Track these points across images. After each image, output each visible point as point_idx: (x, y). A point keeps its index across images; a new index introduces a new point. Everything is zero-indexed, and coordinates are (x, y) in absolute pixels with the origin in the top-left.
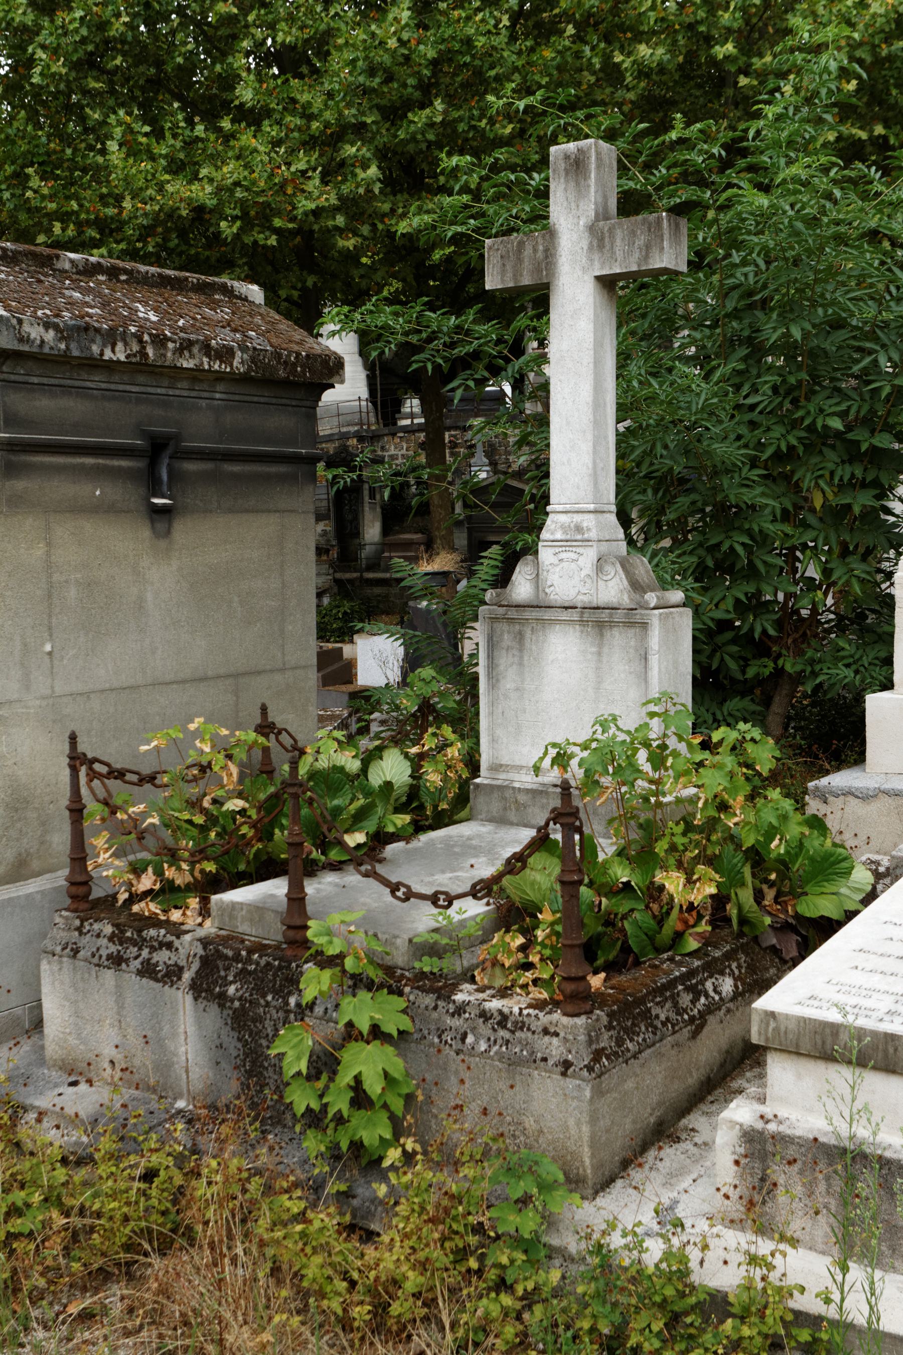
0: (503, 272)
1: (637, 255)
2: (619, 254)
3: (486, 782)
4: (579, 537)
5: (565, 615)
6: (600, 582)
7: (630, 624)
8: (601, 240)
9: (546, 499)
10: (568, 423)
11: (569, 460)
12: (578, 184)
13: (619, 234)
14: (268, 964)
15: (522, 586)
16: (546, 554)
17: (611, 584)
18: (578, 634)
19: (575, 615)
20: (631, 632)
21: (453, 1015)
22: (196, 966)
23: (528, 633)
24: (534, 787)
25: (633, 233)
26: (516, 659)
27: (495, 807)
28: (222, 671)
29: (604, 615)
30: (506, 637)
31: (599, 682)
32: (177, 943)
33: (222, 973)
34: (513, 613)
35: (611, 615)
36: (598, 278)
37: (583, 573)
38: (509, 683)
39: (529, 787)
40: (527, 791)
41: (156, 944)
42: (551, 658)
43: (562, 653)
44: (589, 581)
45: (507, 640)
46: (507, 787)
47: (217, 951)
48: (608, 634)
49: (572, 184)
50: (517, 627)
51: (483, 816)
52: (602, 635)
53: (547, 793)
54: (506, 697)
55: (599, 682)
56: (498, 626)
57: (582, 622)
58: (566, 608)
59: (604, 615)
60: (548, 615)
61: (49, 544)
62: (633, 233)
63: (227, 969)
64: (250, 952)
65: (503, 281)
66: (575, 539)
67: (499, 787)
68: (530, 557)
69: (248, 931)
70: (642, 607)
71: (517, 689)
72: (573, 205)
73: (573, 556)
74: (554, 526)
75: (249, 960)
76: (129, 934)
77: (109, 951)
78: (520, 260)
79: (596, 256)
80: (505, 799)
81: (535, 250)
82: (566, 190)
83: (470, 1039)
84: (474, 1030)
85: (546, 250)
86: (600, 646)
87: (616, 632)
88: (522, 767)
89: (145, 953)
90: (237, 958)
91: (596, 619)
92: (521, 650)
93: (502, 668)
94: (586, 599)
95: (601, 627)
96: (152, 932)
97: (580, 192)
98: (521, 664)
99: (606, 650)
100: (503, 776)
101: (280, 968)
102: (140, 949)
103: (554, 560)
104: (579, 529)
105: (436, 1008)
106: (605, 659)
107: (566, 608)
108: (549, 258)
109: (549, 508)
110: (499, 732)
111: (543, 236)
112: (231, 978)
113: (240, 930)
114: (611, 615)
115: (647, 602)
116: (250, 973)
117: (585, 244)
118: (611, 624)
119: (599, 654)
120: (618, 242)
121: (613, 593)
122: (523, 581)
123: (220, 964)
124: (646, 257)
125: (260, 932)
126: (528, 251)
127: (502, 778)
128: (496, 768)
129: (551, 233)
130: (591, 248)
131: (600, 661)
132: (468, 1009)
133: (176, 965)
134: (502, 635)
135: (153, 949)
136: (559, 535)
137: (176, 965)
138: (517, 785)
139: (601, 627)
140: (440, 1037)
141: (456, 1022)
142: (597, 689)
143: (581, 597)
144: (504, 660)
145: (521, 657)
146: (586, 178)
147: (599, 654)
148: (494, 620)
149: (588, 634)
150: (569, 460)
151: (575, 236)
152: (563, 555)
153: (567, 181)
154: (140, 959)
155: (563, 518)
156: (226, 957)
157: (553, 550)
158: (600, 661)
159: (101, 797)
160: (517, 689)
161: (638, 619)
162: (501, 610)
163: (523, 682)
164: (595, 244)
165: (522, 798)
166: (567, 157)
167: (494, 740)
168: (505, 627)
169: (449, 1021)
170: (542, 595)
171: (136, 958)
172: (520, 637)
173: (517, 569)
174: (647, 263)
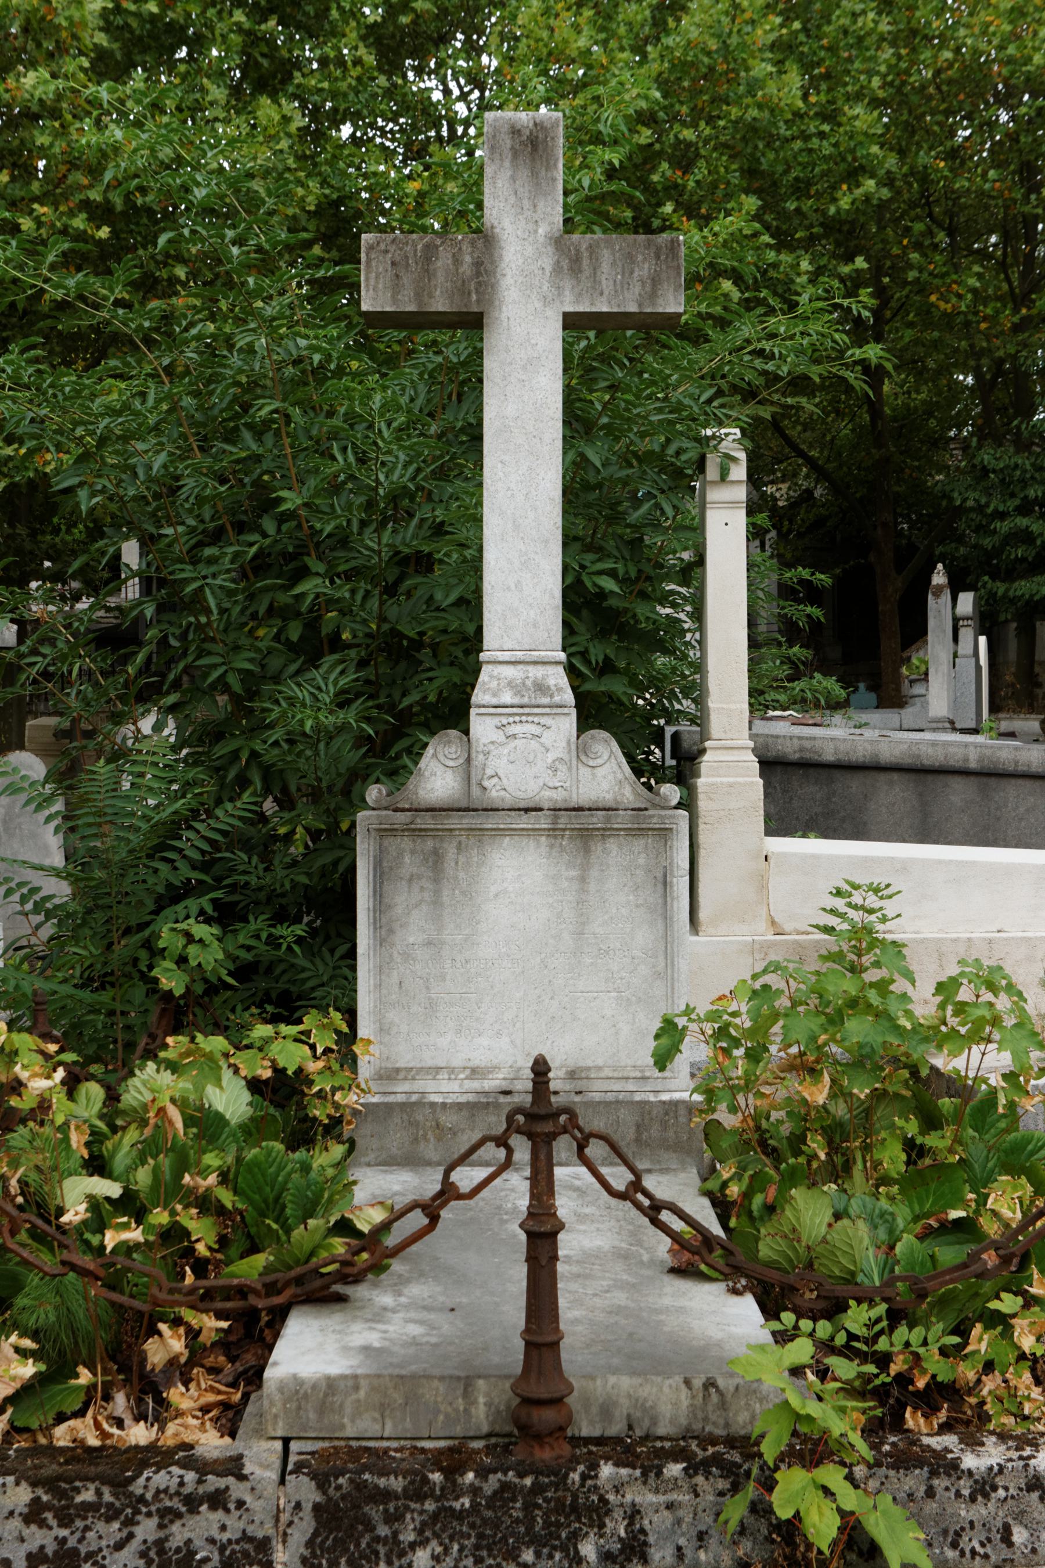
0: (396, 285)
1: (637, 289)
2: (606, 285)
4: (545, 700)
5: (524, 822)
6: (583, 771)
8: (575, 262)
9: (474, 641)
10: (517, 527)
11: (518, 585)
12: (534, 173)
13: (606, 256)
14: (505, 1486)
15: (437, 775)
16: (481, 727)
17: (600, 772)
18: (544, 850)
19: (543, 821)
20: (639, 844)
21: (973, 1499)
22: (303, 1529)
23: (450, 850)
25: (630, 258)
27: (396, 1139)
29: (597, 820)
30: (407, 860)
32: (238, 1490)
33: (383, 1531)
34: (425, 821)
35: (608, 820)
36: (566, 315)
37: (551, 757)
38: (413, 932)
40: (459, 1106)
41: (176, 1504)
42: (493, 889)
43: (515, 884)
44: (563, 768)
45: (409, 864)
46: (419, 1104)
47: (359, 1486)
48: (597, 848)
49: (524, 173)
50: (430, 843)
51: (371, 1157)
52: (587, 851)
54: (407, 957)
56: (393, 844)
57: (554, 832)
58: (527, 810)
59: (597, 820)
60: (490, 822)
62: (630, 258)
63: (394, 1518)
64: (452, 1472)
65: (394, 300)
66: (530, 706)
67: (403, 1106)
68: (453, 733)
69: (375, 1429)
71: (429, 943)
72: (526, 204)
74: (493, 686)
75: (452, 1489)
76: (88, 1496)
77: (33, 1546)
78: (428, 272)
79: (567, 284)
80: (415, 1124)
81: (457, 261)
82: (513, 179)
83: (1019, 1535)
84: (1020, 1516)
85: (478, 264)
86: (585, 868)
87: (612, 844)
88: (438, 1069)
89: (146, 1529)
90: (419, 1491)
92: (437, 881)
93: (399, 910)
95: (585, 836)
96: (161, 1479)
97: (538, 187)
98: (437, 903)
99: (594, 873)
100: (405, 1087)
101: (537, 1489)
102: (130, 1522)
103: (499, 736)
104: (541, 688)
105: (930, 1493)
106: (592, 887)
107: (527, 810)
108: (483, 273)
109: (483, 656)
110: (392, 1015)
111: (473, 243)
112: (408, 1536)
113: (350, 1432)
114: (608, 820)
115: (666, 799)
116: (460, 1515)
117: (547, 262)
118: (606, 833)
119: (583, 879)
120: (605, 267)
121: (605, 785)
122: (439, 770)
123: (374, 1512)
124: (653, 295)
125: (408, 1427)
126: (443, 260)
127: (401, 1091)
128: (390, 1075)
129: (484, 238)
130: (557, 269)
131: (583, 891)
132: (1000, 1481)
133: (245, 1537)
134: (400, 855)
135: (168, 1516)
136: (507, 698)
137: (245, 1537)
138: (438, 1099)
139: (585, 836)
140: (954, 1545)
141: (980, 1511)
142: (579, 934)
143: (547, 794)
144: (401, 898)
145: (437, 893)
146: (550, 167)
147: (583, 879)
148: (386, 832)
150: (518, 585)
151: (530, 250)
152: (517, 729)
153: (515, 166)
154: (135, 1545)
155: (509, 672)
156: (387, 1495)
157: (496, 721)
158: (583, 891)
159: (620, 1186)
160: (429, 943)
162: (402, 818)
164: (565, 264)
165: (448, 1120)
166: (515, 131)
168: (406, 843)
169: (965, 1512)
170: (476, 791)
171: (119, 1546)
172: (436, 859)
174: (654, 305)
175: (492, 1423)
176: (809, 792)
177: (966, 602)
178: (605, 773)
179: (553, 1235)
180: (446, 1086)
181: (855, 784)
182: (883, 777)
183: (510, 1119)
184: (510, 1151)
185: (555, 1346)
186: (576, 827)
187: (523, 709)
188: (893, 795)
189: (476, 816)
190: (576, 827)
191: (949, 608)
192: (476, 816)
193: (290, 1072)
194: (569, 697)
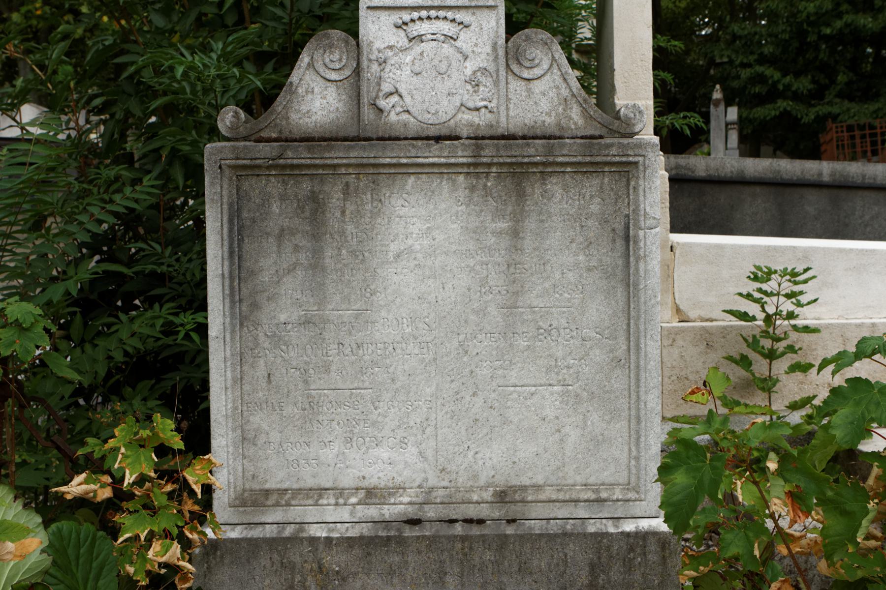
3: (234, 534)
5: (434, 155)
6: (516, 85)
7: (589, 168)
15: (315, 96)
17: (538, 87)
18: (462, 193)
24: (365, 530)
26: (303, 257)
28: (472, 135)
29: (534, 151)
31: (515, 292)
34: (298, 155)
35: (550, 151)
37: (470, 67)
38: (286, 306)
39: (354, 532)
40: (349, 542)
42: (394, 248)
46: (294, 540)
48: (535, 191)
50: (306, 186)
52: (521, 195)
53: (401, 541)
54: (277, 340)
55: (515, 292)
56: (254, 186)
57: (475, 169)
58: (438, 139)
61: (492, 502)
67: (272, 543)
70: (613, 133)
71: (307, 322)
73: (446, 28)
86: (518, 217)
87: (555, 186)
91: (504, 163)
93: (265, 277)
94: (481, 119)
98: (316, 266)
99: (531, 224)
103: (399, 39)
106: (528, 243)
107: (438, 139)
110: (258, 420)
114: (550, 151)
118: (547, 169)
119: (515, 233)
122: (318, 85)
127: (271, 522)
128: (254, 499)
134: (266, 200)
142: (510, 307)
143: (467, 117)
145: (317, 253)
147: (515, 233)
148: (245, 171)
149: (487, 192)
158: (516, 248)
160: (307, 322)
161: (614, 155)
162: (266, 150)
163: (321, 303)
165: (334, 560)
167: (246, 439)
168: (274, 186)
170: (368, 114)
172: (314, 209)
173: (305, 58)
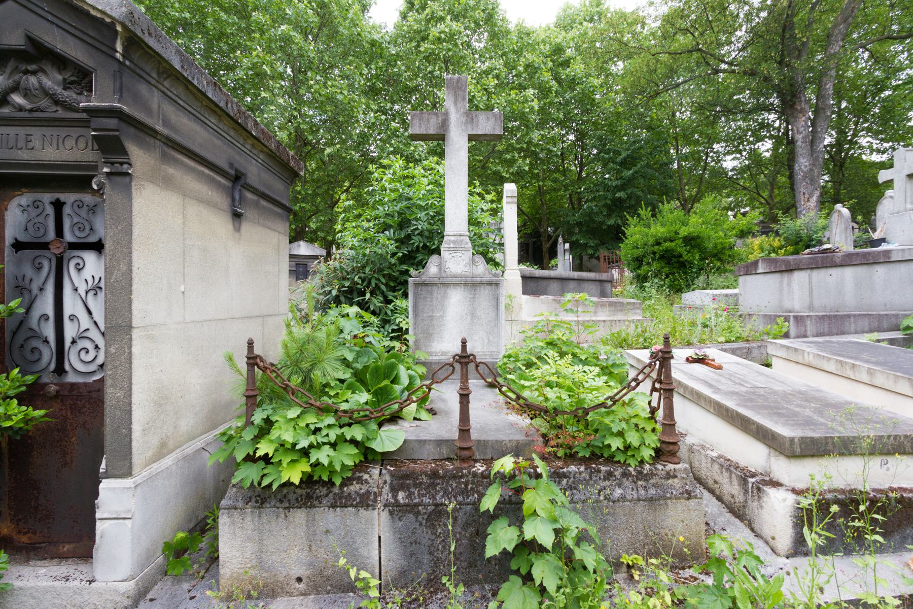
0: (420, 127)
15: (432, 267)
43: (455, 302)
155: (452, 238)
175: (445, 297)
176: (532, 284)
177: (567, 246)
178: (481, 268)
179: (468, 395)
180: (434, 358)
181: (544, 283)
182: (551, 281)
183: (454, 358)
184: (454, 368)
185: (468, 430)
186: (471, 284)
187: (455, 249)
188: (554, 286)
189: (444, 283)
190: (471, 284)
191: (563, 247)
192: (444, 283)
193: (491, 510)
194: (470, 245)
